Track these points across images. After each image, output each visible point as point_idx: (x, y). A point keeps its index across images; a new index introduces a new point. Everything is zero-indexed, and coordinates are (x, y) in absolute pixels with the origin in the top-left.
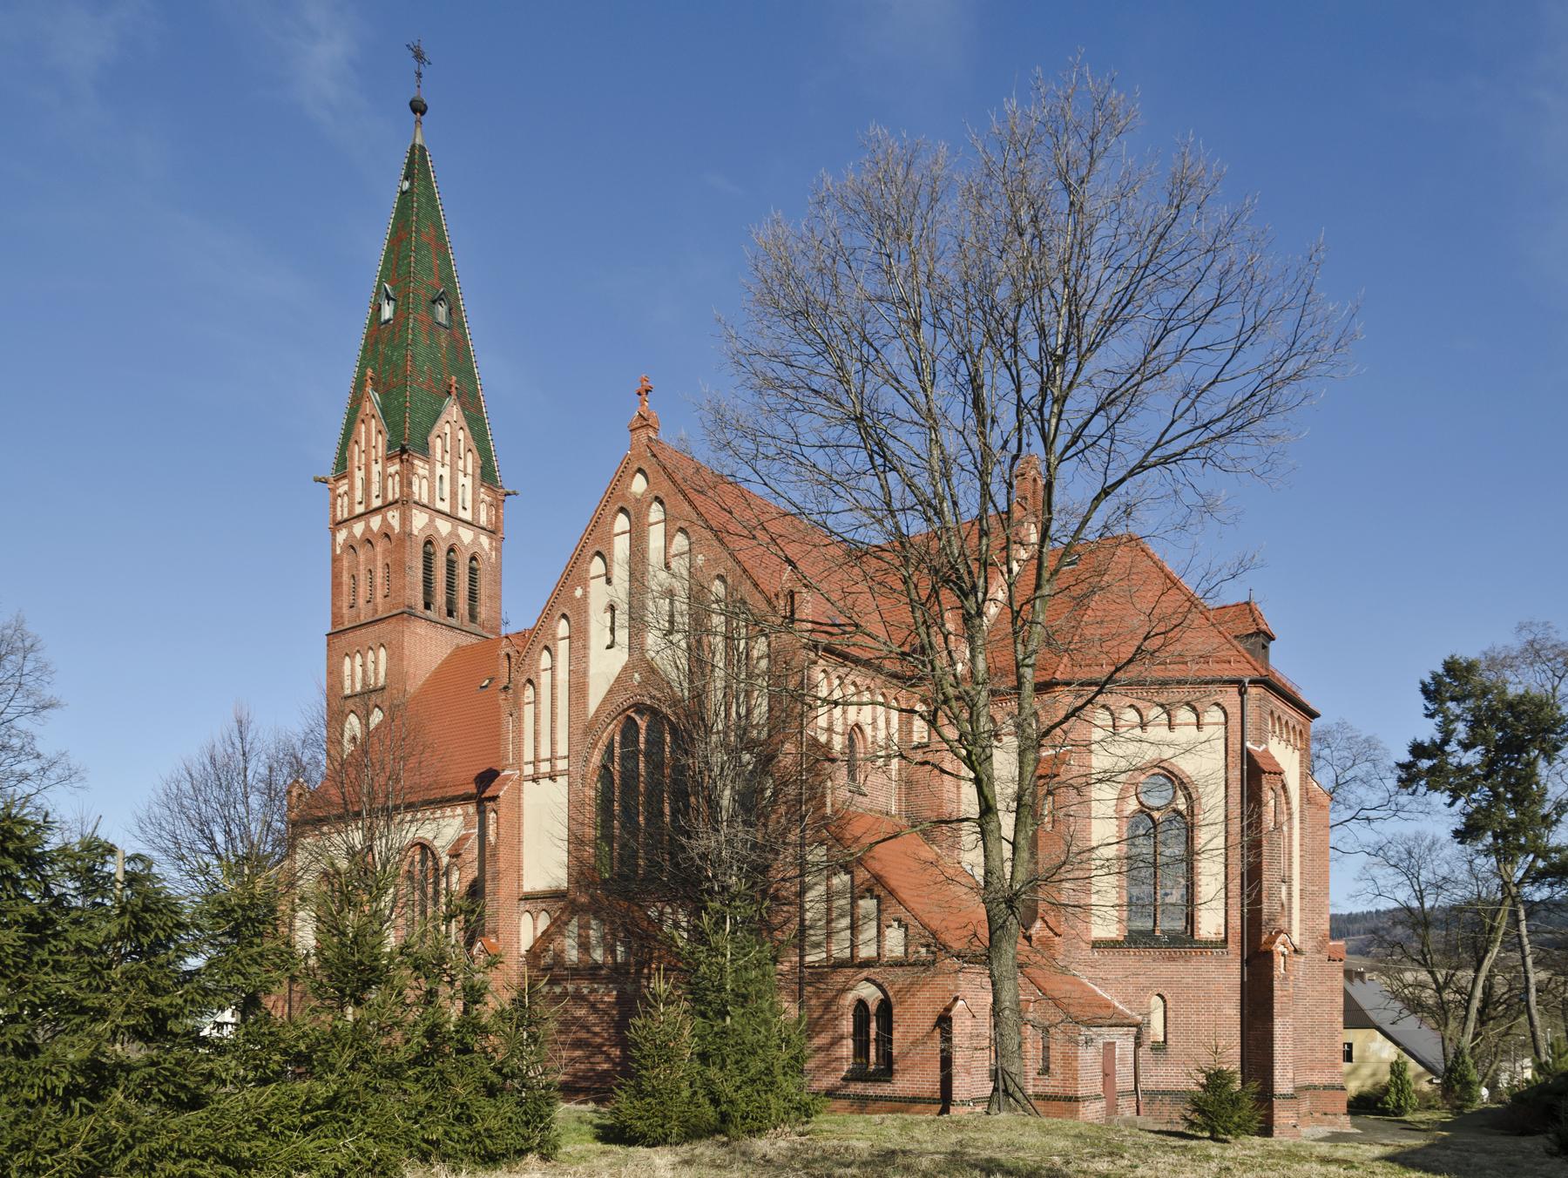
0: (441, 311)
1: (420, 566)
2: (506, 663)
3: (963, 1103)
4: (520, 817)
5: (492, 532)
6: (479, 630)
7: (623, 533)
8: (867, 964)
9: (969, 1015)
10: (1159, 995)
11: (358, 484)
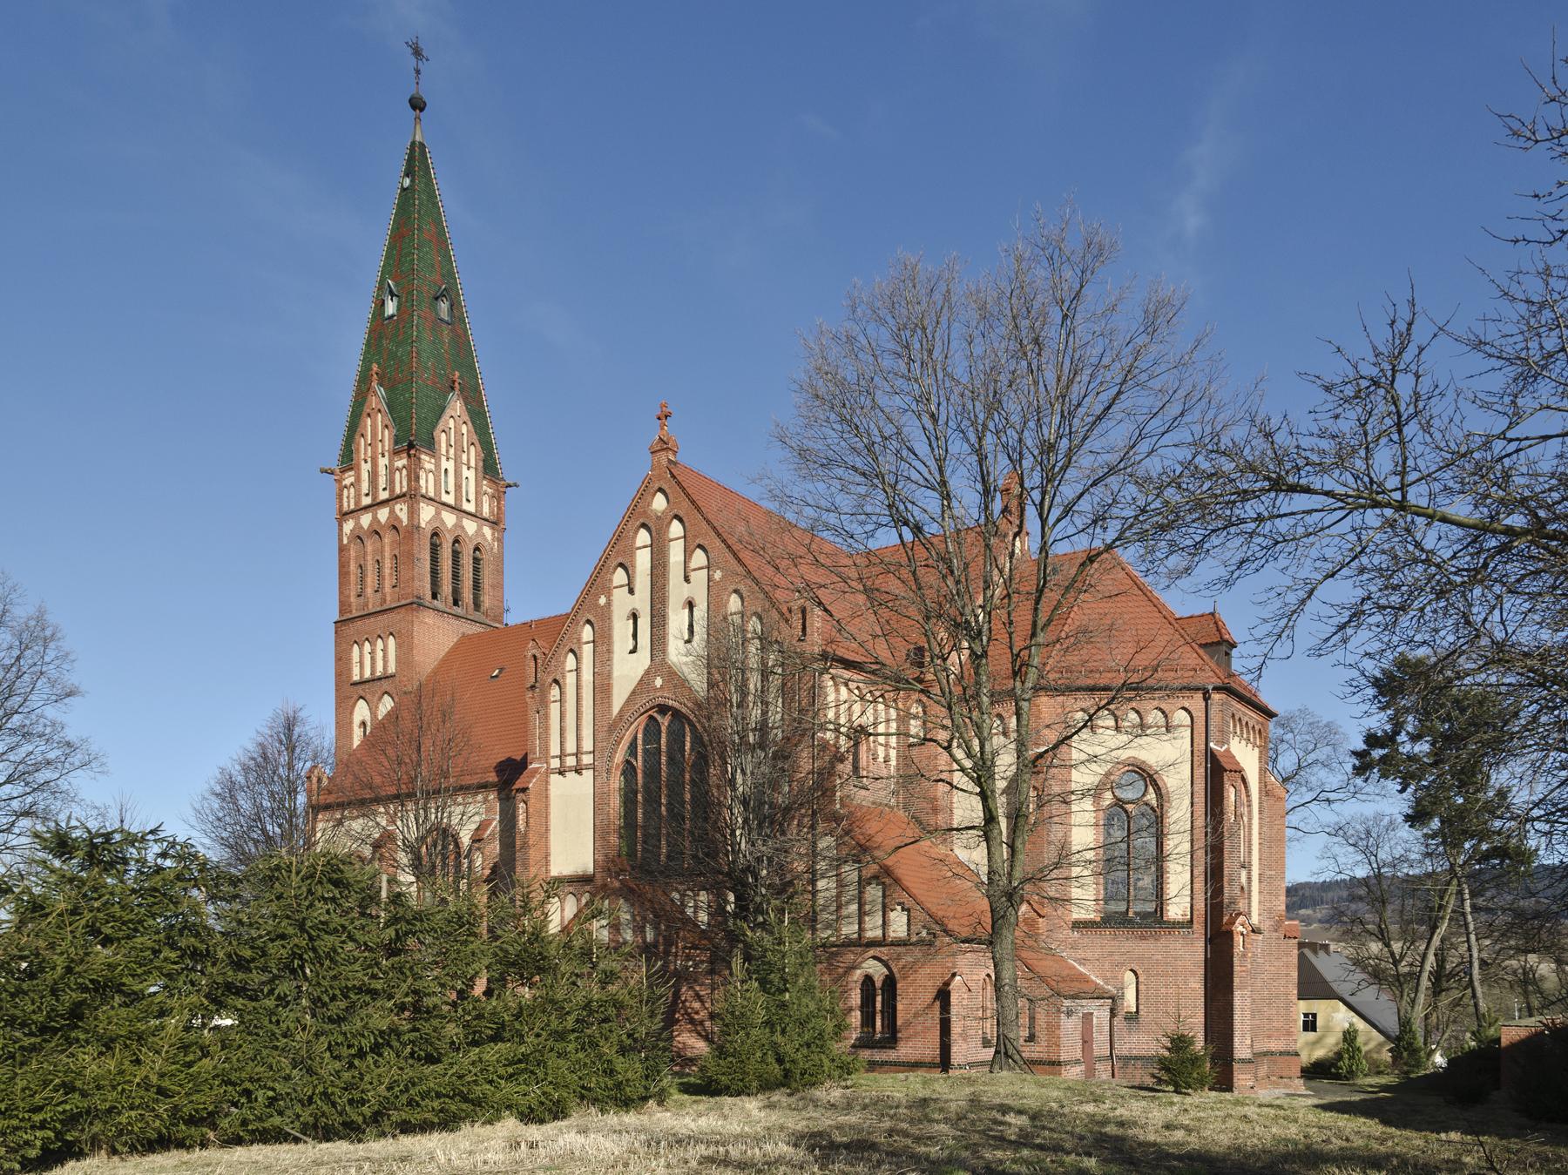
0: (444, 306)
1: (428, 558)
2: (533, 663)
3: (960, 1067)
4: (547, 806)
5: (494, 523)
6: (483, 619)
7: (645, 547)
8: (873, 943)
9: (965, 989)
10: (1132, 970)
11: (365, 476)
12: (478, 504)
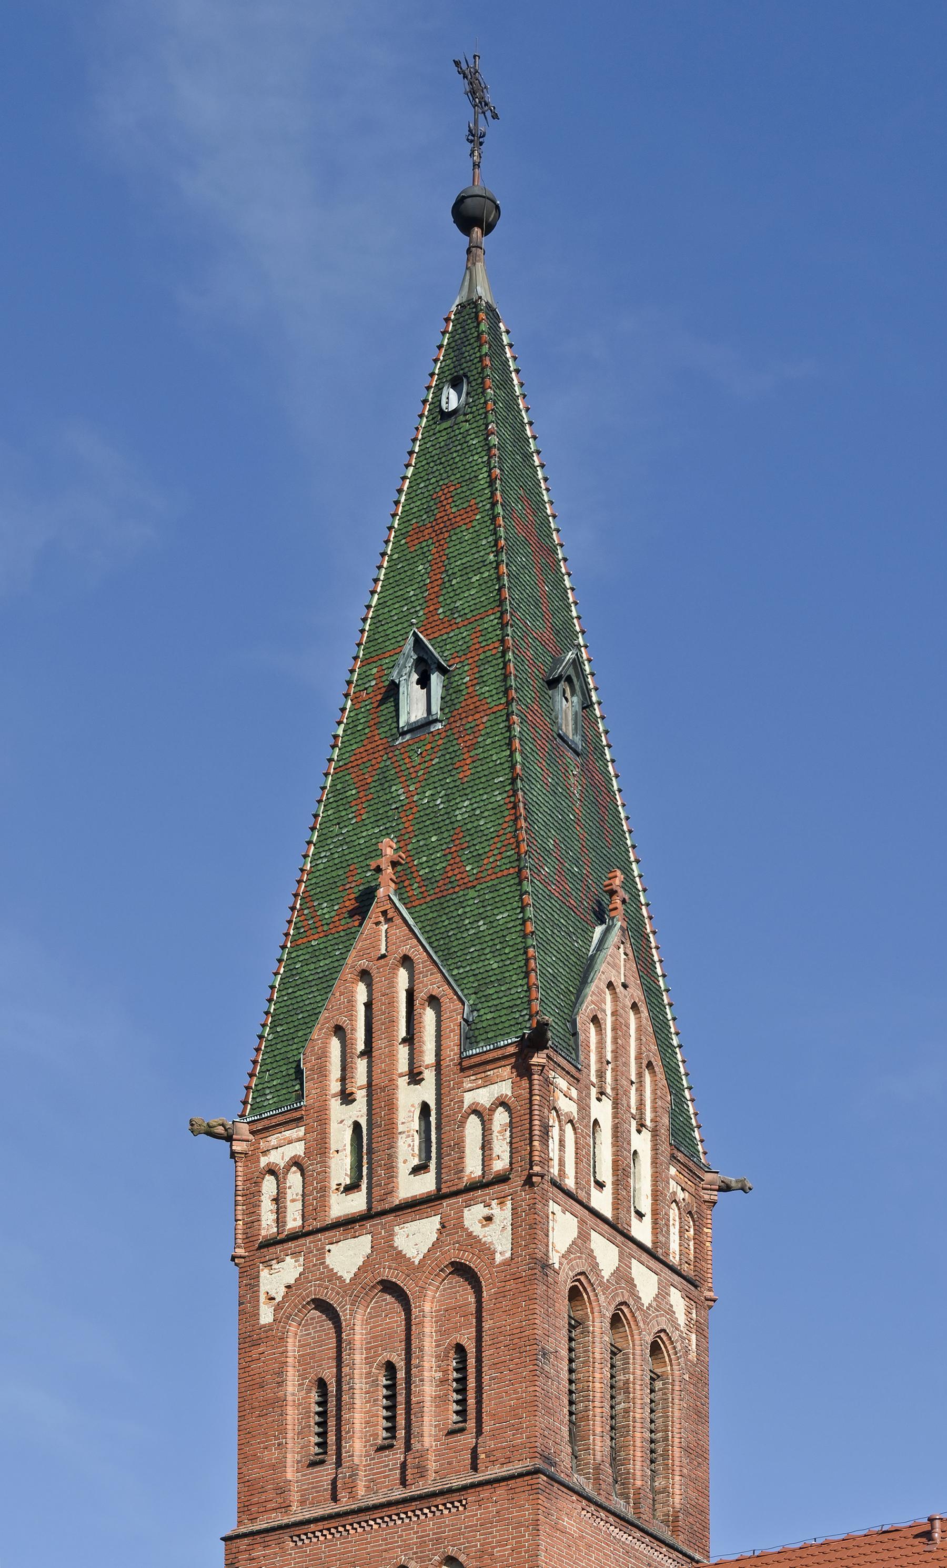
12: (659, 1226)
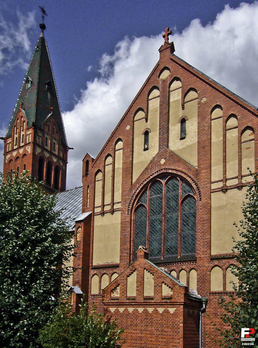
12: (59, 152)
